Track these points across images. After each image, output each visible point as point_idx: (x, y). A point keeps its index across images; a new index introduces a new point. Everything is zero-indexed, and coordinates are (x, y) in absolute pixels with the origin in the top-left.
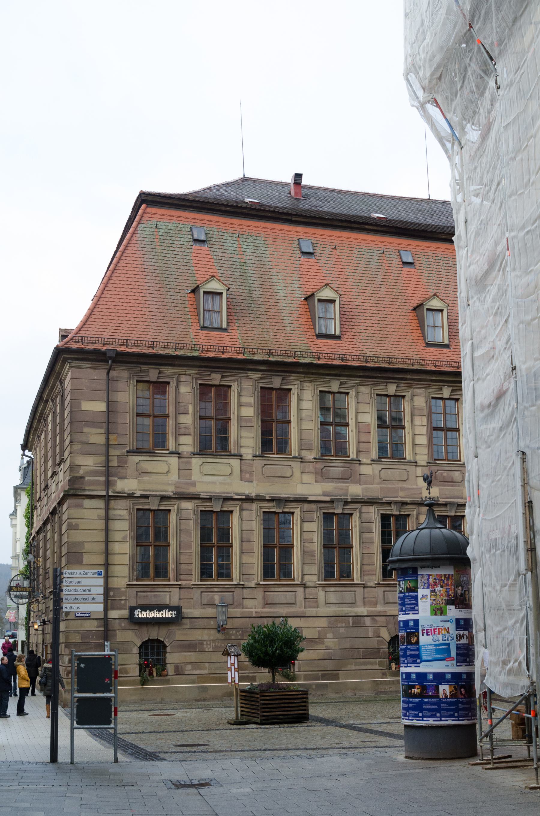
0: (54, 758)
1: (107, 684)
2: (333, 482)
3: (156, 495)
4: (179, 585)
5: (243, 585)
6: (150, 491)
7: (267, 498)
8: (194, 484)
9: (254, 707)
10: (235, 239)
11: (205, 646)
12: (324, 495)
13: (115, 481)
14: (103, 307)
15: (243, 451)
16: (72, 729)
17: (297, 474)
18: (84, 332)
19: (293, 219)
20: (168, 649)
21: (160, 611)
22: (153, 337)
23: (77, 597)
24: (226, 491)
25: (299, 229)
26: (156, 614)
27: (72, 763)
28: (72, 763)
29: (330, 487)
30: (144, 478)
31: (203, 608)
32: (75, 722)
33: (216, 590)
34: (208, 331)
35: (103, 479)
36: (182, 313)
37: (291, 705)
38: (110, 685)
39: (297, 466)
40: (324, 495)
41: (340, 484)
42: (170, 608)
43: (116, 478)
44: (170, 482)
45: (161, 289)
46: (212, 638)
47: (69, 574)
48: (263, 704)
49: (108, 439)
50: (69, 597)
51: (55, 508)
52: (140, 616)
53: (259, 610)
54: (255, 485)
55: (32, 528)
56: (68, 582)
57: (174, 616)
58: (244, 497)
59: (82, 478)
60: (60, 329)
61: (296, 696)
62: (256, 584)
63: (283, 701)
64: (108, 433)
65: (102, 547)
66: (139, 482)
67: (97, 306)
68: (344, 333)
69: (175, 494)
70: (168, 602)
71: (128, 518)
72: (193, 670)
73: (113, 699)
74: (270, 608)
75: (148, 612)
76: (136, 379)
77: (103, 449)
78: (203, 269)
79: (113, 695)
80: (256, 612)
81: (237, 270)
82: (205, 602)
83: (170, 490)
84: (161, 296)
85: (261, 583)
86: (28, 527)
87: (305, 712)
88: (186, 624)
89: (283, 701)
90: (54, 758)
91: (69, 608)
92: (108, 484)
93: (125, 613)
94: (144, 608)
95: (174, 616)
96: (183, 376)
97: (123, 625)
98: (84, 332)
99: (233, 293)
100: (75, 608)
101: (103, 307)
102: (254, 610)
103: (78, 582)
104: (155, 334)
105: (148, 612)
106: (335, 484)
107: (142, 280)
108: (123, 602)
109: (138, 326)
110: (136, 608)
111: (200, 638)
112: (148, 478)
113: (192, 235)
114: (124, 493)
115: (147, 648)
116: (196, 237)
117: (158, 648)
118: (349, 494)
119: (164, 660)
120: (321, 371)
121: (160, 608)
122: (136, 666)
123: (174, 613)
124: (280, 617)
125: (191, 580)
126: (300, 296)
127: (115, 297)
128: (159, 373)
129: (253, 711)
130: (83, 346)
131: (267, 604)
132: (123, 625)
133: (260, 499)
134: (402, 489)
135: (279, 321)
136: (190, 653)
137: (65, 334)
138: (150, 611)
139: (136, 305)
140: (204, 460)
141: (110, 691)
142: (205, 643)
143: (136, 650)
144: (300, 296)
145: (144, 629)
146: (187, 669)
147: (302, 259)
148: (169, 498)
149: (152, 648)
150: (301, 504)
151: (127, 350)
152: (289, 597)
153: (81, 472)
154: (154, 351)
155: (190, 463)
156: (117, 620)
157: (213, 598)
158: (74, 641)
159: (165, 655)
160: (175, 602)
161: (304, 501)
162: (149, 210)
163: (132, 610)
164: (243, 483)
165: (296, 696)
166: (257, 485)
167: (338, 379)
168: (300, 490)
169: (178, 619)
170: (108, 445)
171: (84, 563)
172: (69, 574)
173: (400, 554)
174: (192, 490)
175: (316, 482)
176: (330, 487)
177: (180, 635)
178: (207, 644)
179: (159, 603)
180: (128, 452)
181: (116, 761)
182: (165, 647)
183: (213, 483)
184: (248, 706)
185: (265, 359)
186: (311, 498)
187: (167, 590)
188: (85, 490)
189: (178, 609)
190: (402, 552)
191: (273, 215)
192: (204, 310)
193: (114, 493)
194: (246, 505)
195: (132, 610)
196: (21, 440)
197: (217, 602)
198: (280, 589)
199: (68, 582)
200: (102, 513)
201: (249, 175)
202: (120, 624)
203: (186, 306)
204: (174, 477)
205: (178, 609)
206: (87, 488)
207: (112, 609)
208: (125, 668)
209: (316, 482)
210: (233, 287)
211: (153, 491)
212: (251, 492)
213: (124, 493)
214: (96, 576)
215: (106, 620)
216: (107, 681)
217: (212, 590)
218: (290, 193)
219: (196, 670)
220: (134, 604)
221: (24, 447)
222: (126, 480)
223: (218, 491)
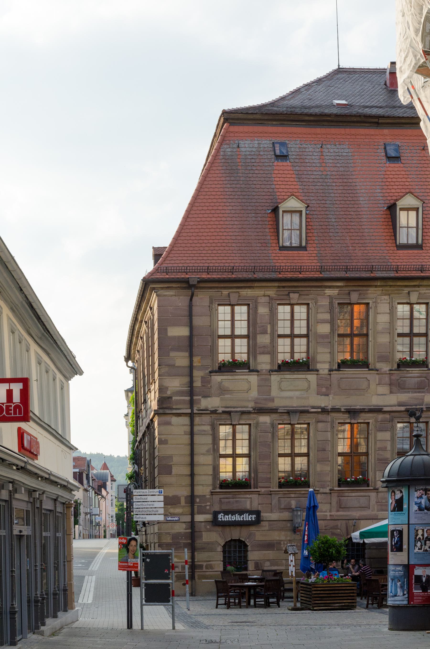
0: (130, 625)
1: (166, 573)
2: (408, 392)
3: (236, 412)
4: (259, 491)
5: (318, 491)
6: (231, 407)
7: (343, 410)
8: (272, 400)
9: (309, 596)
10: (318, 150)
11: (282, 546)
12: (400, 405)
13: (200, 400)
14: (186, 234)
15: (319, 366)
16: (142, 605)
17: (373, 386)
18: (168, 262)
19: (380, 121)
20: (249, 548)
21: (241, 515)
22: (233, 261)
23: (144, 509)
24: (303, 405)
25: (386, 131)
26: (237, 518)
27: (142, 629)
28: (142, 629)
29: (404, 397)
30: (226, 396)
31: (280, 512)
32: (144, 600)
33: (293, 495)
34: (288, 250)
35: (188, 398)
36: (262, 234)
37: (340, 595)
38: (169, 574)
40: (400, 405)
41: (415, 394)
42: (251, 512)
43: (200, 397)
44: (250, 399)
45: (242, 212)
46: (288, 538)
47: (138, 493)
48: (315, 594)
49: (191, 361)
50: (138, 510)
51: (149, 424)
52: (223, 520)
53: (333, 513)
54: (331, 398)
55: (137, 436)
56: (136, 499)
57: (253, 519)
58: (320, 410)
59: (170, 398)
60: (153, 248)
61: (345, 588)
62: (330, 490)
63: (334, 592)
64: (191, 356)
65: (188, 459)
66: (222, 400)
67: (181, 235)
68: (426, 241)
69: (254, 409)
70: (248, 507)
71: (211, 432)
72: (271, 566)
73: (171, 584)
74: (343, 511)
75: (230, 516)
76: (217, 303)
77: (187, 371)
78: (284, 187)
79: (171, 581)
80: (330, 515)
81: (319, 184)
82: (282, 506)
83: (250, 406)
84: (243, 219)
85: (335, 489)
86: (134, 435)
87: (121, 564)
88: (265, 526)
89: (334, 592)
90: (130, 625)
91: (138, 518)
92: (192, 403)
93: (209, 517)
94: (226, 513)
95: (253, 519)
96: (263, 298)
97: (208, 527)
98: (168, 262)
99: (313, 209)
100: (142, 518)
101: (186, 234)
102: (328, 514)
103: (144, 499)
104: (235, 258)
105: (230, 516)
106: (410, 395)
107: (223, 204)
108: (208, 507)
109: (219, 252)
110: (219, 513)
111: (278, 538)
112: (229, 396)
113: (274, 151)
114: (207, 410)
115: (230, 547)
116: (278, 152)
117: (240, 547)
118: (425, 403)
119: (246, 557)
120: (399, 283)
121: (241, 513)
122: (220, 562)
123: (254, 516)
124: (354, 520)
125: (270, 487)
126: (383, 205)
127: (197, 223)
128: (239, 296)
129: (308, 599)
130: (167, 276)
131: (341, 507)
132: (208, 527)
133: (335, 410)
135: (359, 234)
136: (269, 552)
137: (157, 253)
138: (232, 515)
139: (218, 230)
140: (282, 376)
141: (169, 579)
142: (282, 543)
143: (220, 549)
144: (383, 205)
145: (227, 529)
146: (266, 565)
147: (387, 165)
148: (249, 413)
149: (235, 547)
150: (375, 415)
151: (209, 276)
152: (363, 501)
153: (169, 393)
154: (233, 276)
155: (269, 380)
156: (203, 523)
157: (289, 503)
158: (166, 541)
159: (246, 553)
160: (255, 506)
161: (378, 410)
162: (232, 129)
163: (215, 514)
164: (319, 397)
165: (345, 588)
166: (333, 398)
167: (417, 291)
168: (375, 401)
169: (258, 521)
170: (191, 367)
171: (173, 473)
172: (138, 493)
173: (389, 476)
174: (270, 405)
175: (391, 392)
176: (404, 397)
177: (260, 534)
178: (284, 544)
179: (240, 508)
180: (210, 372)
181: (174, 628)
182: (246, 546)
183: (291, 398)
184: (305, 595)
185: (343, 275)
186: (385, 409)
187: (248, 496)
188: (172, 409)
189: (258, 513)
190: (390, 474)
191: (359, 119)
192: (283, 230)
193: (198, 410)
194: (321, 417)
195: (215, 514)
196: (124, 352)
197: (293, 506)
198: (354, 494)
199: (136, 499)
200: (188, 429)
201: (344, 65)
202: (205, 526)
203: (267, 226)
204: (254, 394)
205: (258, 513)
206: (174, 407)
207: (199, 513)
208: (211, 564)
209: (391, 392)
210: (314, 202)
211: (234, 408)
212: (327, 405)
213: (207, 410)
214: (158, 494)
215: (192, 524)
216: (166, 571)
217: (288, 496)
218: (385, 84)
219: (274, 566)
220: (217, 508)
221: (127, 359)
222: (209, 399)
223: (295, 405)
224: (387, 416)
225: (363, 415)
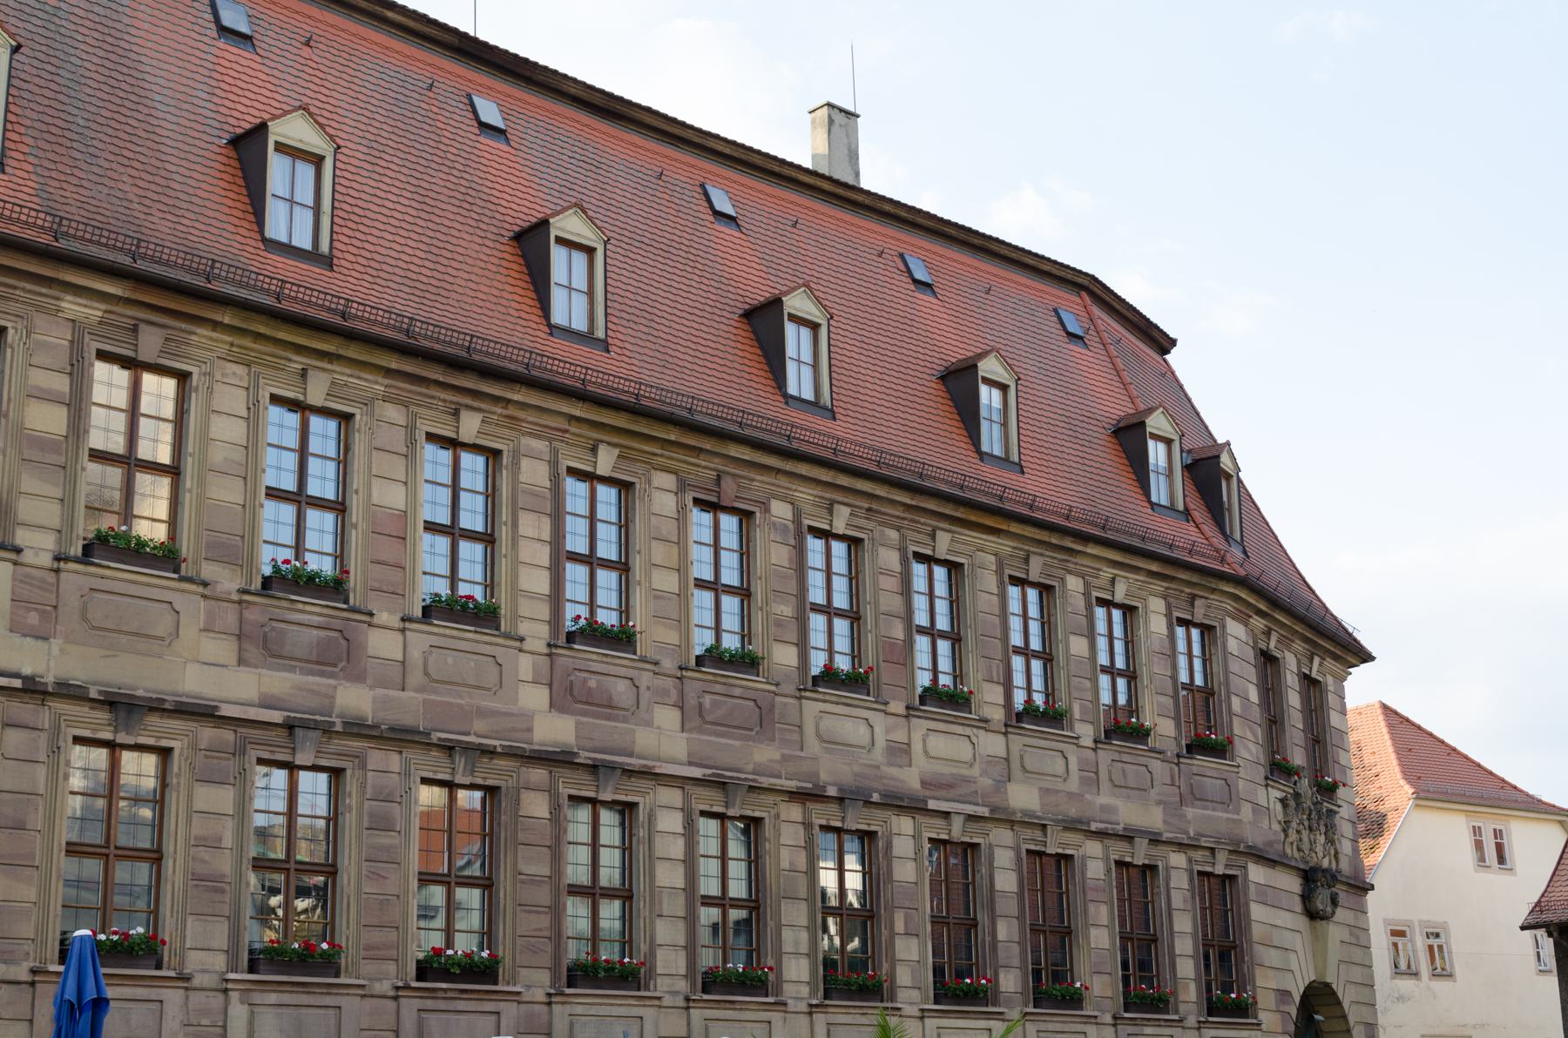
29: (280, 681)
39: (191, 605)
133: (68, 692)
134: (482, 713)
168: (194, 683)
186: (227, 710)
224: (228, 735)
225: (154, 720)
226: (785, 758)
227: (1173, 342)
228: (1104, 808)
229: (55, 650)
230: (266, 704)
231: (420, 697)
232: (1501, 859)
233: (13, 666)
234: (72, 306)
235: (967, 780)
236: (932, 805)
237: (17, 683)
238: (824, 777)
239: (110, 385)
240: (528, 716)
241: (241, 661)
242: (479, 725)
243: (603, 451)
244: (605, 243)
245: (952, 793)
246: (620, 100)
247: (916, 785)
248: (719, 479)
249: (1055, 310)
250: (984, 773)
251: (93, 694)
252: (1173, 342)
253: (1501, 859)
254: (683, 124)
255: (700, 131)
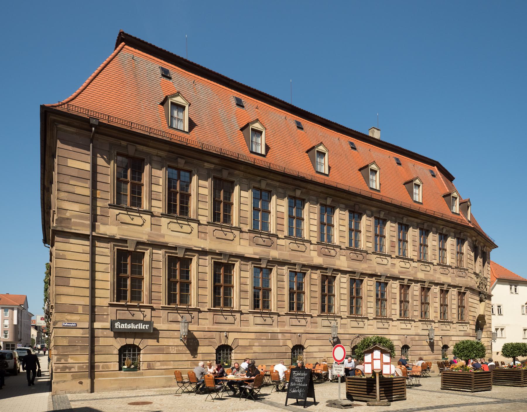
29: (259, 249)
134: (302, 257)
226: (369, 267)
227: (454, 178)
228: (438, 278)
229: (208, 242)
230: (255, 254)
231: (289, 253)
232: (516, 292)
233: (199, 246)
234: (207, 165)
235: (408, 272)
236: (401, 277)
237: (200, 249)
238: (377, 271)
239: (185, 176)
240: (312, 257)
241: (249, 245)
242: (302, 259)
243: (328, 199)
244: (189, 106)
245: (405, 274)
246: (329, 121)
247: (397, 273)
248: (355, 205)
249: (126, 39)
250: (412, 270)
251: (217, 252)
252: (454, 178)
253: (516, 292)
254: (344, 127)
255: (347, 128)
